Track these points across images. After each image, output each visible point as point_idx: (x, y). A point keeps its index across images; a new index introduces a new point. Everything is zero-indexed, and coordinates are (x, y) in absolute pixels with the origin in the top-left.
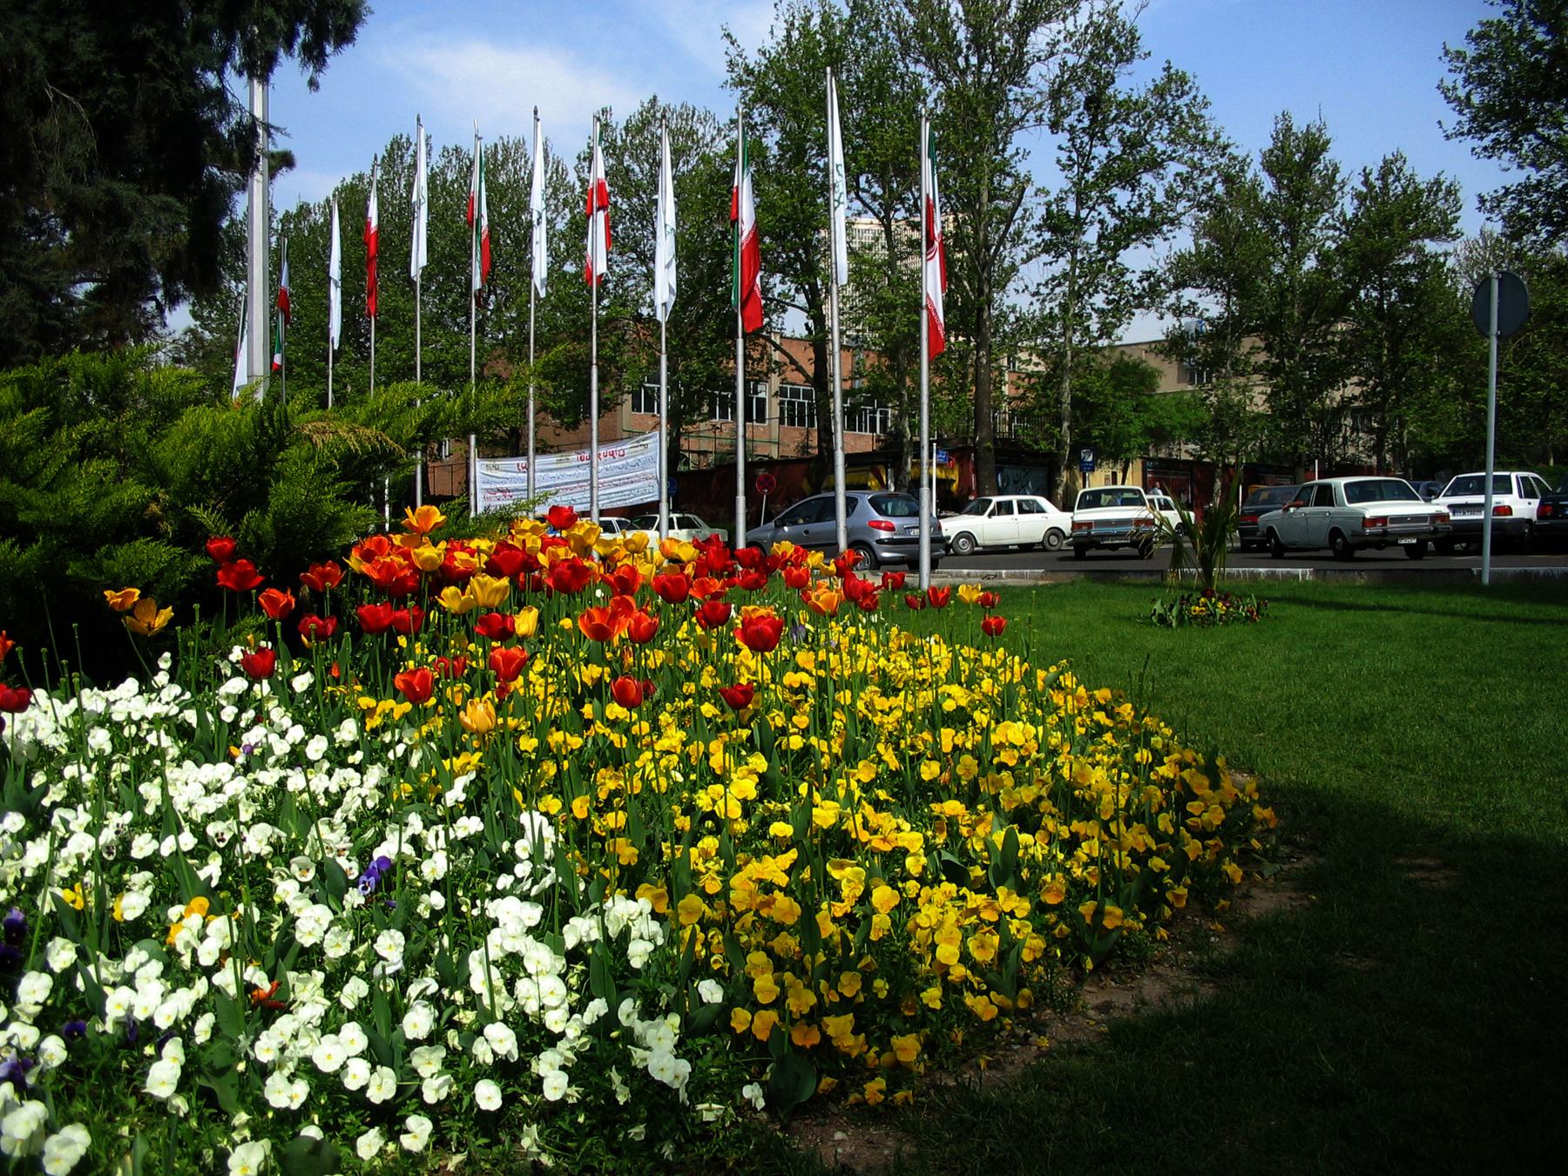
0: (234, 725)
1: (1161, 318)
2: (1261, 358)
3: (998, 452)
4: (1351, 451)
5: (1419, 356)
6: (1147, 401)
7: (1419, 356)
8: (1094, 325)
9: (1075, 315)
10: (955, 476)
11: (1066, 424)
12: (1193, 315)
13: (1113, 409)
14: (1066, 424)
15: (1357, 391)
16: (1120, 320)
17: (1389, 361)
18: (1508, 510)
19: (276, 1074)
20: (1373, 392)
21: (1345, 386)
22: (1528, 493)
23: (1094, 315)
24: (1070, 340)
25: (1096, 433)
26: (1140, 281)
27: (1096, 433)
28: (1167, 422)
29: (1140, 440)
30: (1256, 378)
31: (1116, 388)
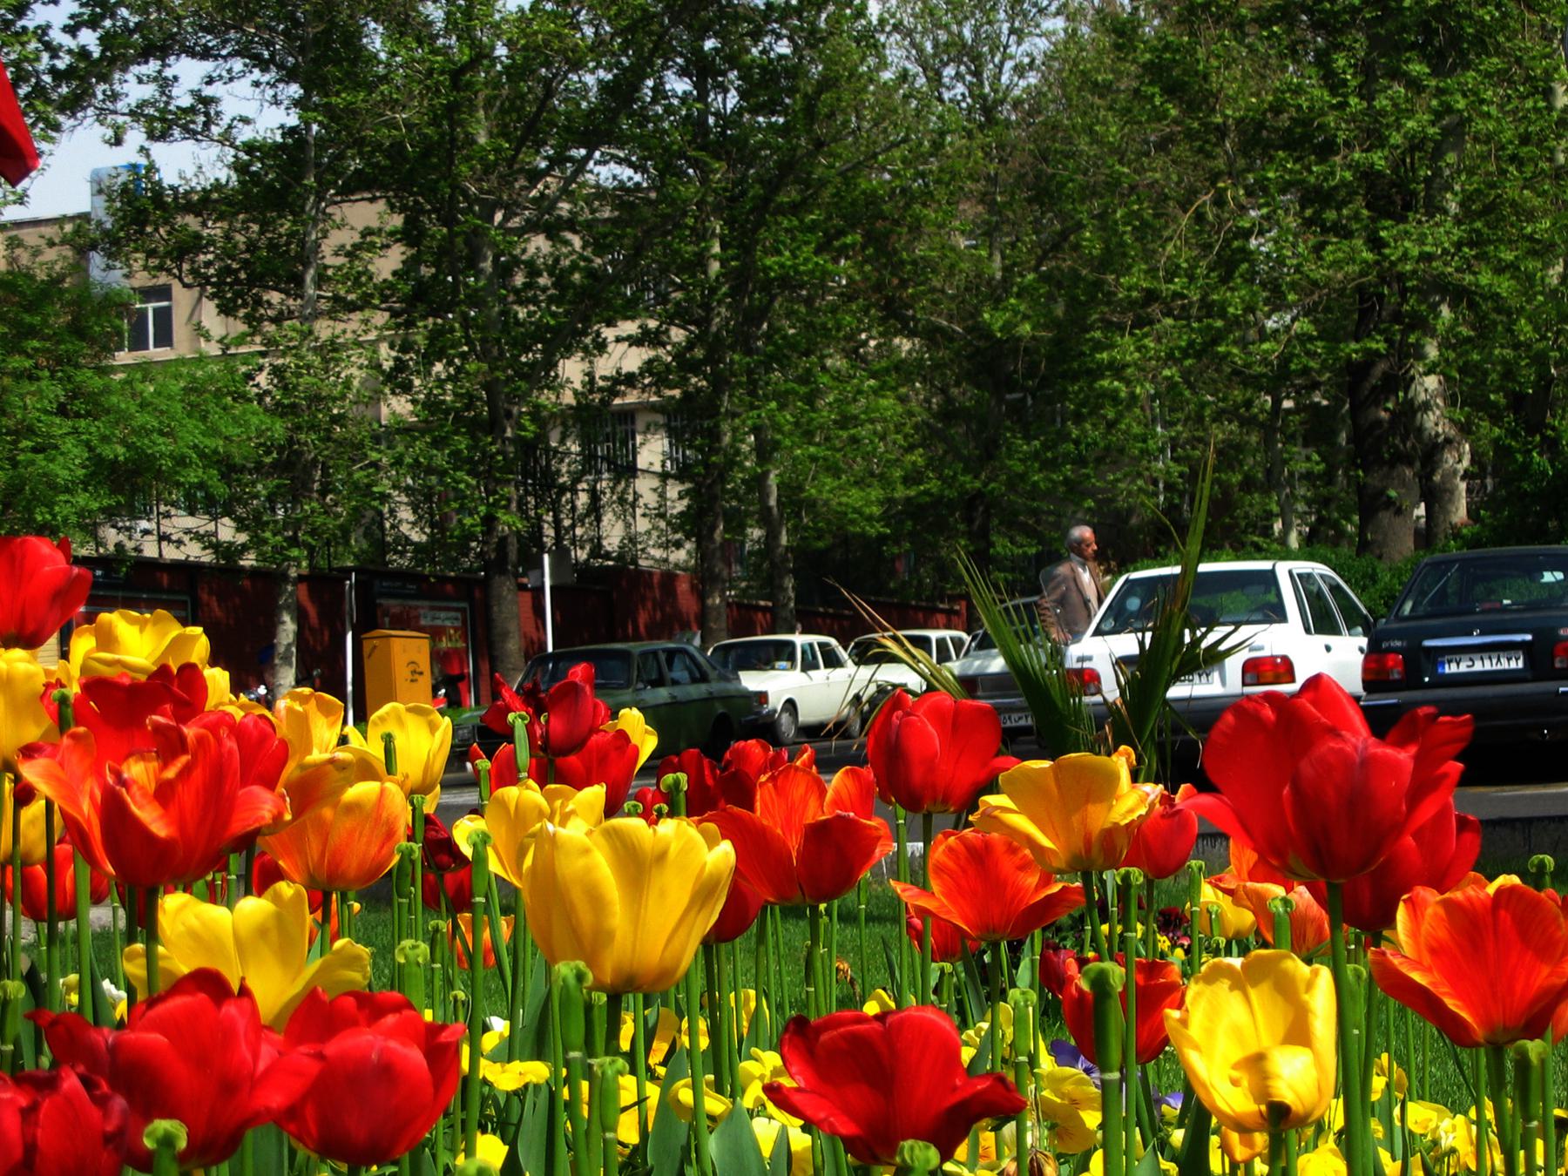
1: (118, 141)
4: (613, 535)
5: (808, 258)
6: (97, 383)
7: (808, 258)
15: (633, 360)
17: (726, 274)
18: (1284, 669)
20: (685, 362)
21: (601, 347)
22: (1321, 621)
26: (71, 30)
28: (163, 445)
29: (82, 499)
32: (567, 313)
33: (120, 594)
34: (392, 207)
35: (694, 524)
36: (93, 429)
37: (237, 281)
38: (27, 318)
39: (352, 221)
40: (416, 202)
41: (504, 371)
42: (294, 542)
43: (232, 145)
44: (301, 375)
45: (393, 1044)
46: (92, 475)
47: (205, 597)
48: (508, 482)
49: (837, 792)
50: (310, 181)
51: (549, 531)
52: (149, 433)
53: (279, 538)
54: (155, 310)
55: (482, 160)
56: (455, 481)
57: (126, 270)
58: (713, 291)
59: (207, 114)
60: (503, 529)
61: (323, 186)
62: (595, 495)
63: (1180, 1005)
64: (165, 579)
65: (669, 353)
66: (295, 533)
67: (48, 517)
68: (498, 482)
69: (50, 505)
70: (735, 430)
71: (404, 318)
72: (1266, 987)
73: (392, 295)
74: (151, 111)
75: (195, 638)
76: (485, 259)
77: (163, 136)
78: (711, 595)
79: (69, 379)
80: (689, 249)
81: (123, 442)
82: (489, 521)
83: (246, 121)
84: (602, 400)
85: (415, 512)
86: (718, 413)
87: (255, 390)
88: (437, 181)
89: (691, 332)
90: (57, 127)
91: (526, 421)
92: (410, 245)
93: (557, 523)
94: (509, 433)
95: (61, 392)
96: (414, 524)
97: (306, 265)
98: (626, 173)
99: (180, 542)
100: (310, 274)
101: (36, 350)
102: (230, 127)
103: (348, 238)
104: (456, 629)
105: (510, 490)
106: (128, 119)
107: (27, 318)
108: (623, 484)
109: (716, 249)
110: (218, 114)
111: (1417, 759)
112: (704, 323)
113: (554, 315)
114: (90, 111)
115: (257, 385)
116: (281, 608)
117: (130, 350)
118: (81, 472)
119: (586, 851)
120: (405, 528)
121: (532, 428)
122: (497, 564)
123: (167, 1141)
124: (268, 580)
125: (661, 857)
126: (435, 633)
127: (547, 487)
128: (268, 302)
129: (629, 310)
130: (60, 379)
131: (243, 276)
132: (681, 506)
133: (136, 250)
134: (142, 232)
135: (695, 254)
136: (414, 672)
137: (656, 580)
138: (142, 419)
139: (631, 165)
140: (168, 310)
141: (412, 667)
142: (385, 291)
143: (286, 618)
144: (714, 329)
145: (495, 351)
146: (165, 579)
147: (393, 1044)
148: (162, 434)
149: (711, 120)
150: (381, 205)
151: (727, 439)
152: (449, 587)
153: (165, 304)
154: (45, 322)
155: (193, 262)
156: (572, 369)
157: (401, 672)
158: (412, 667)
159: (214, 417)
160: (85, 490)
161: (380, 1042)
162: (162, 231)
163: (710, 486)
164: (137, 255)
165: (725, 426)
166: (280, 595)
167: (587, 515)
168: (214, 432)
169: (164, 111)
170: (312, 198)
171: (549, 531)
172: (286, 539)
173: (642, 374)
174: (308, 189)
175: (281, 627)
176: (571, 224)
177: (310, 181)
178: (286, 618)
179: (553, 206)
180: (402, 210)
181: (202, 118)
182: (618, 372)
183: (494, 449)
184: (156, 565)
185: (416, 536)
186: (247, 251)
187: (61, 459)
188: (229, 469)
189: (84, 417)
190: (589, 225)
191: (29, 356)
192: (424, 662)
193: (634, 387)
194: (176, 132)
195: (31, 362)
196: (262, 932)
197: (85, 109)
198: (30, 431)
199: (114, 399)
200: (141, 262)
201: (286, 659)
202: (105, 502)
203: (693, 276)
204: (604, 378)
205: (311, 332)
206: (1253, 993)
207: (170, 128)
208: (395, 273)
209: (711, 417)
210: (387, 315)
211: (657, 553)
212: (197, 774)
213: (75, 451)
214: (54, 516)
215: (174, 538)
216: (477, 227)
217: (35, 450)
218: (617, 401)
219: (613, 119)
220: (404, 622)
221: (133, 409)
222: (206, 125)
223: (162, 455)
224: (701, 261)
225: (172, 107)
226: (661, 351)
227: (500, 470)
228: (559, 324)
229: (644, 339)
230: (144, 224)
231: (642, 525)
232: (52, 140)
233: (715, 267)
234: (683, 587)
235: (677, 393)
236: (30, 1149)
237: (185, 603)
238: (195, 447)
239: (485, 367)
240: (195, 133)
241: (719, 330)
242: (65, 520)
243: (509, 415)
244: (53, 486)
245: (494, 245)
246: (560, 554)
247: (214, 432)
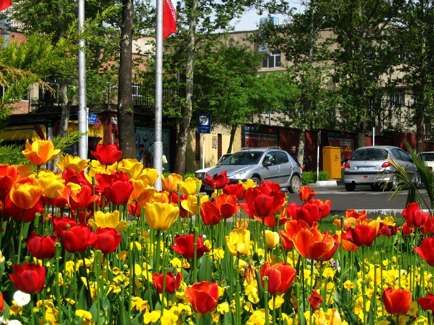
0: (74, 76)
1: (261, 14)
2: (333, 47)
3: (136, 116)
4: (394, 122)
6: (252, 78)
8: (213, 17)
9: (198, 9)
10: (101, 135)
11: (189, 95)
12: (284, 12)
13: (226, 84)
14: (189, 95)
15: (401, 75)
16: (232, 14)
17: (427, 52)
19: (111, 25)
21: (392, 71)
23: (214, 10)
24: (194, 29)
25: (213, 103)
27: (213, 103)
28: (268, 95)
29: (246, 109)
30: (330, 62)
31: (230, 67)
32: (382, 63)
33: (259, 134)
34: (335, 32)
35: (416, 120)
36: (250, 90)
37: (293, 51)
38: (234, 61)
39: (323, 36)
40: (342, 32)
41: (364, 77)
42: (304, 122)
43: (291, 15)
44: (308, 78)
45: (109, 235)
46: (250, 103)
47: (281, 135)
48: (364, 107)
49: (228, 199)
50: (312, 25)
51: (377, 121)
52: (265, 92)
53: (300, 121)
54: (276, 57)
55: (359, 20)
56: (348, 107)
57: (263, 48)
58: (423, 57)
59: (285, 7)
60: (362, 120)
61: (315, 26)
62: (390, 111)
63: (228, 235)
64: (271, 130)
65: (411, 74)
66: (305, 120)
67: (237, 113)
68: (361, 107)
69: (238, 110)
70: (427, 95)
71: (337, 63)
72: (242, 233)
73: (334, 56)
74: (270, 6)
75: (140, 165)
76: (360, 47)
77: (273, 12)
78: (419, 140)
79: (245, 77)
80: (416, 46)
81: (258, 94)
82: (358, 118)
83: (296, 9)
84: (392, 86)
85: (341, 114)
86: (423, 91)
87: (296, 81)
88: (347, 26)
89: (417, 68)
90: (243, 10)
91: (369, 91)
92: (339, 43)
93: (379, 119)
94: (365, 94)
95: (242, 80)
96: (340, 118)
97: (310, 48)
98: (400, 24)
99: (276, 121)
100: (311, 50)
101: (236, 69)
102: (291, 10)
103: (322, 41)
104: (350, 147)
105: (365, 110)
106: (264, 8)
107: (234, 61)
108: (398, 108)
109: (424, 46)
110: (288, 7)
111: (274, 199)
112: (420, 66)
113: (378, 63)
114: (254, 5)
115: (296, 80)
116: (300, 139)
117: (269, 67)
118: (246, 102)
119: (152, 207)
120: (338, 119)
121: (371, 93)
122: (360, 129)
123: (57, 245)
124: (298, 131)
125: (164, 209)
126: (344, 147)
127: (378, 108)
128: (301, 57)
129: (401, 61)
130: (242, 77)
131: (295, 50)
132: (413, 115)
133: (266, 42)
134: (268, 37)
135: (418, 47)
136: (336, 158)
137: (406, 135)
138: (263, 88)
139: (402, 22)
140: (280, 57)
141: (336, 156)
142: (332, 56)
143: (302, 142)
144: (423, 68)
145: (362, 72)
146: (271, 130)
147: (109, 235)
148: (268, 92)
149: (424, 11)
150: (332, 32)
151: (425, 98)
152: (348, 135)
153: (279, 55)
154: (239, 62)
155: (281, 46)
156: (384, 77)
157: (333, 158)
158: (336, 156)
159: (282, 88)
160: (247, 107)
161: (107, 235)
162: (273, 37)
163: (420, 110)
164: (266, 44)
165: (425, 94)
166: (300, 136)
167: (388, 116)
168: (282, 92)
169: (274, 6)
170: (312, 30)
171: (377, 121)
172: (302, 121)
173: (403, 79)
174: (311, 28)
175: (300, 145)
176: (385, 37)
177: (312, 25)
178: (302, 142)
179: (380, 33)
180: (338, 33)
181: (284, 8)
182: (397, 78)
183: (360, 99)
184: (269, 127)
185: (340, 121)
186: (296, 43)
187: (241, 98)
188: (286, 102)
189: (248, 87)
190: (390, 38)
191: (234, 70)
192: (339, 156)
193: (401, 83)
194: (277, 11)
195: (235, 72)
196: (110, 218)
197: (252, 5)
198: (234, 90)
199: (256, 83)
200: (267, 46)
201: (301, 153)
202: (253, 110)
203: (417, 53)
204: (393, 80)
205: (311, 66)
206: (240, 234)
207: (275, 10)
208: (335, 50)
209: (421, 91)
210: (333, 62)
211: (406, 128)
212: (83, 193)
213: (245, 96)
214: (239, 113)
215: (274, 119)
216: (357, 39)
217: (235, 95)
218: (396, 86)
219: (396, 9)
220: (336, 144)
221: (261, 86)
222: (285, 10)
223: (268, 98)
224: (420, 49)
225: (276, 5)
226: (408, 73)
227: (362, 104)
228: (379, 66)
229: (404, 70)
230: (268, 35)
231: (403, 120)
232: (242, 14)
233: (424, 51)
234: (413, 137)
235: (412, 85)
236: (41, 246)
237: (276, 137)
238: (277, 96)
239: (358, 76)
240: (282, 12)
241: (424, 68)
242: (242, 114)
243: (365, 89)
244: (239, 106)
245: (362, 44)
246: (378, 128)
247: (282, 92)
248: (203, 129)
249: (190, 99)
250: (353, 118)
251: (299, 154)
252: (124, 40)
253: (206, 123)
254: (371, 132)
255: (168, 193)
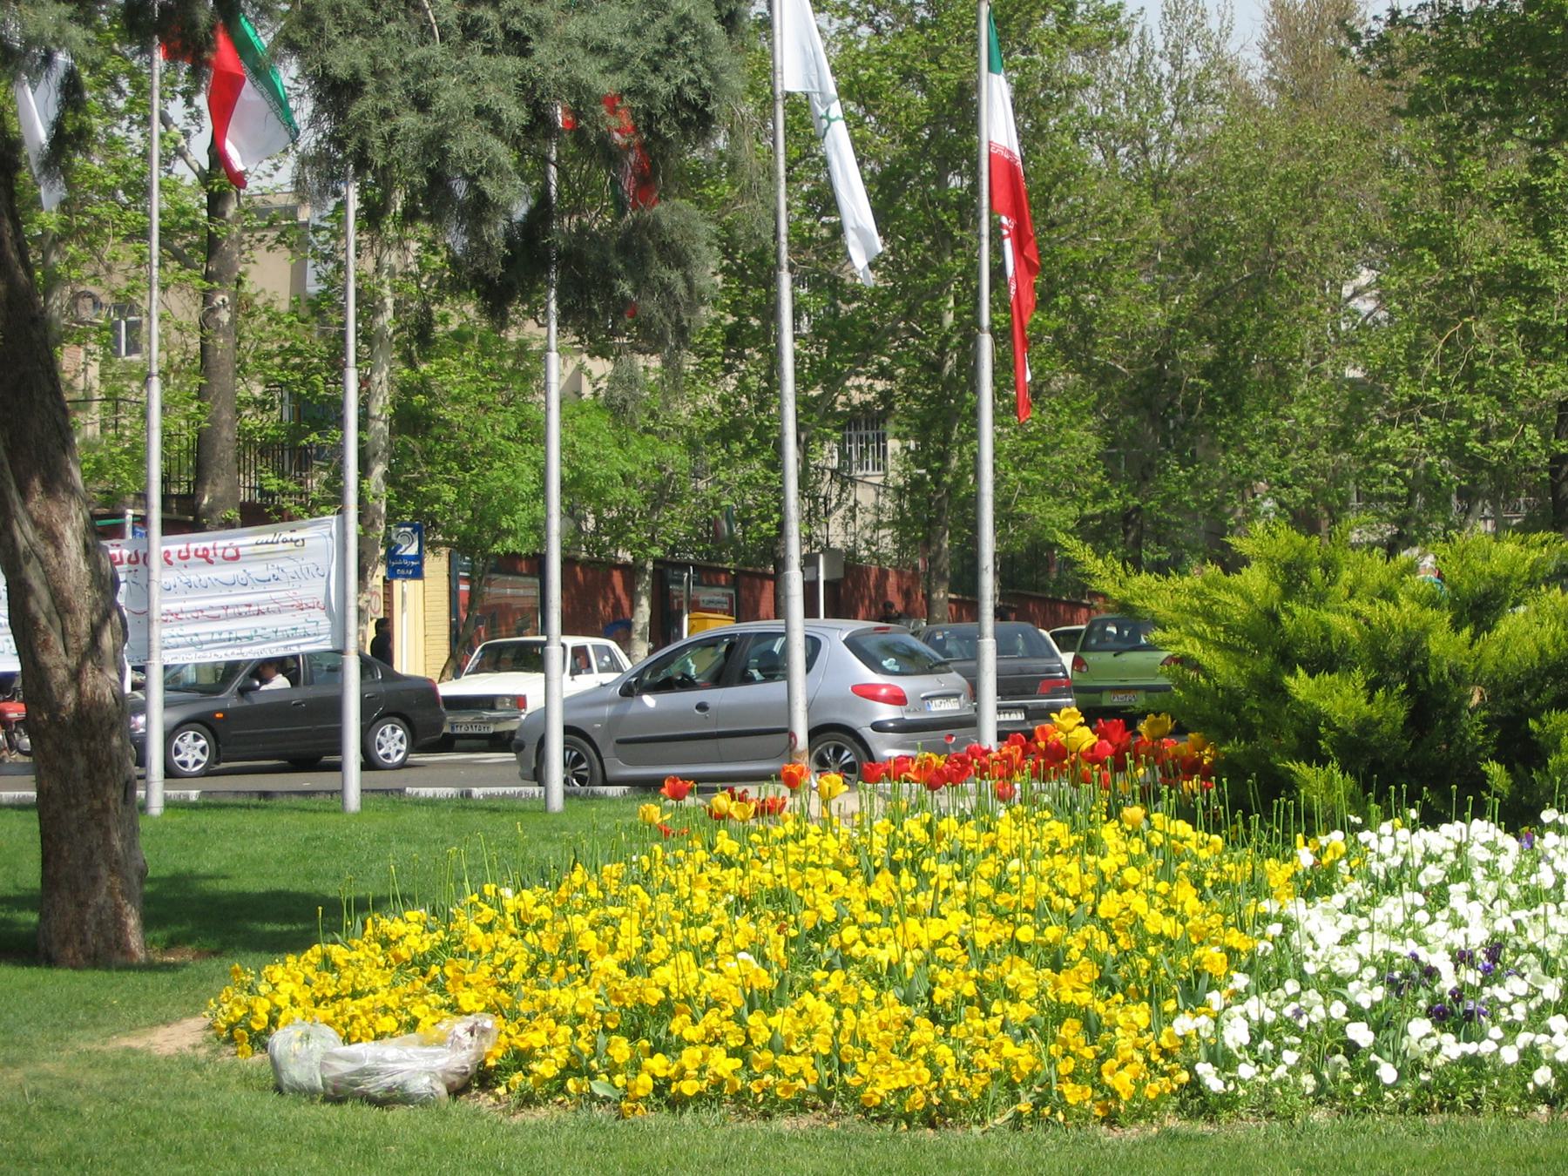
28: (599, 469)
58: (947, 339)
109: (951, 304)
116: (640, 594)
247: (634, 459)
248: (403, 567)
249: (380, 480)
250: (765, 526)
251: (634, 636)
252: (214, 310)
253: (413, 550)
254: (813, 568)
255: (1077, 1024)
